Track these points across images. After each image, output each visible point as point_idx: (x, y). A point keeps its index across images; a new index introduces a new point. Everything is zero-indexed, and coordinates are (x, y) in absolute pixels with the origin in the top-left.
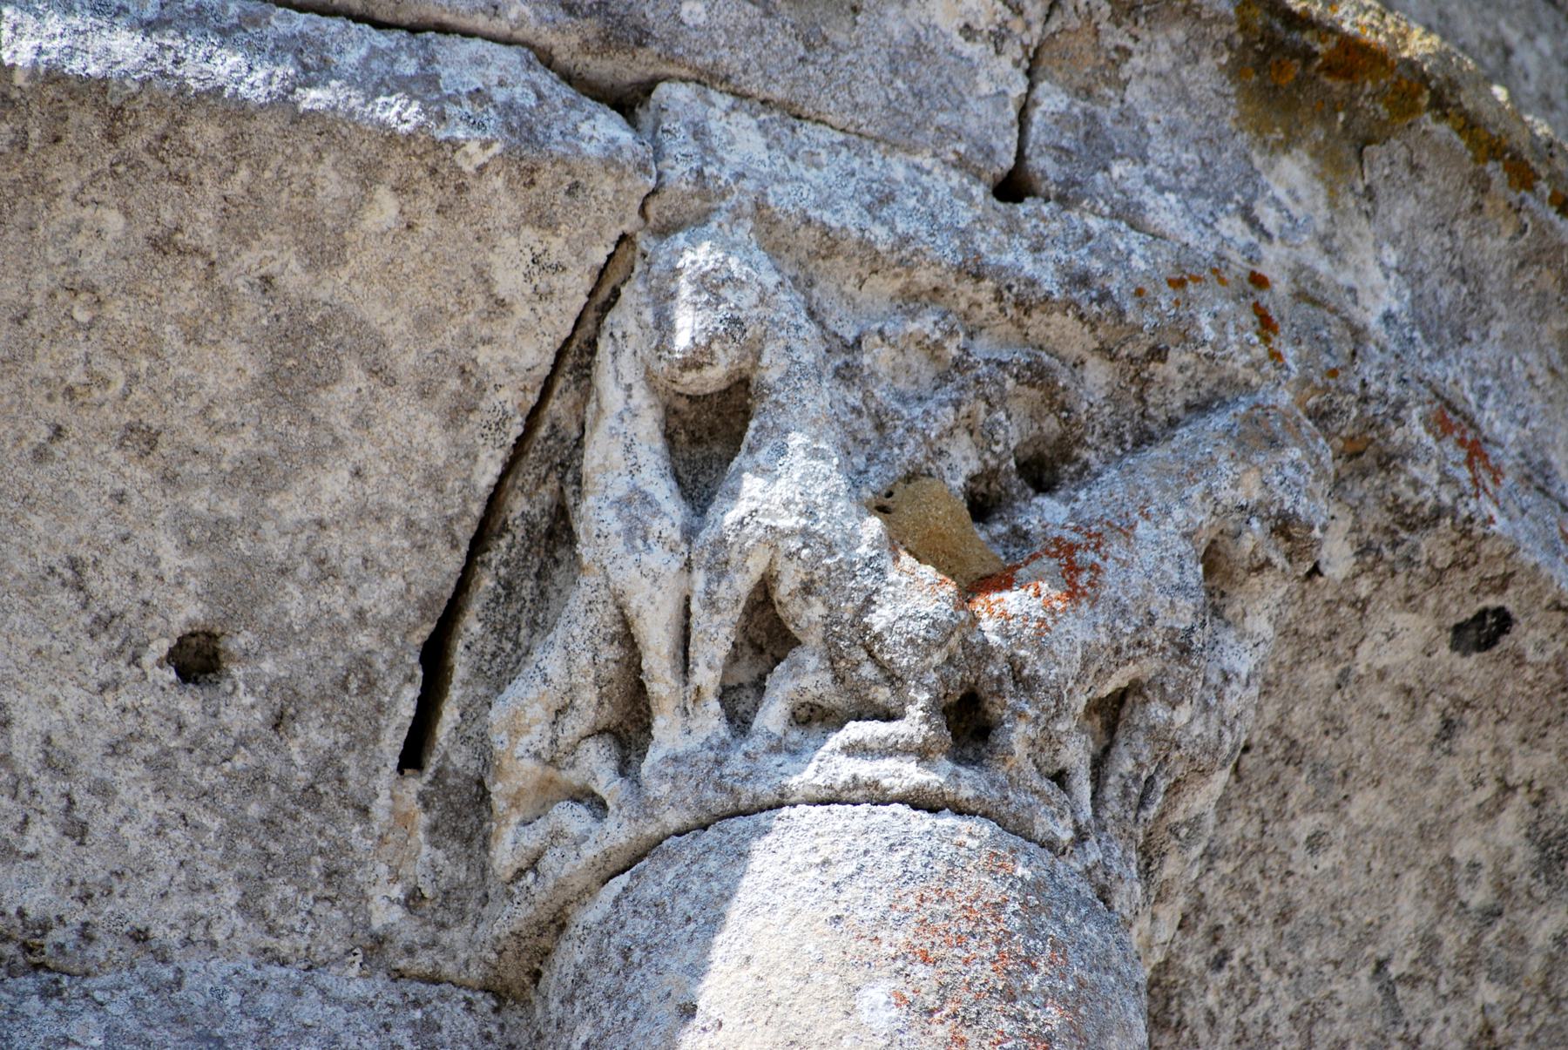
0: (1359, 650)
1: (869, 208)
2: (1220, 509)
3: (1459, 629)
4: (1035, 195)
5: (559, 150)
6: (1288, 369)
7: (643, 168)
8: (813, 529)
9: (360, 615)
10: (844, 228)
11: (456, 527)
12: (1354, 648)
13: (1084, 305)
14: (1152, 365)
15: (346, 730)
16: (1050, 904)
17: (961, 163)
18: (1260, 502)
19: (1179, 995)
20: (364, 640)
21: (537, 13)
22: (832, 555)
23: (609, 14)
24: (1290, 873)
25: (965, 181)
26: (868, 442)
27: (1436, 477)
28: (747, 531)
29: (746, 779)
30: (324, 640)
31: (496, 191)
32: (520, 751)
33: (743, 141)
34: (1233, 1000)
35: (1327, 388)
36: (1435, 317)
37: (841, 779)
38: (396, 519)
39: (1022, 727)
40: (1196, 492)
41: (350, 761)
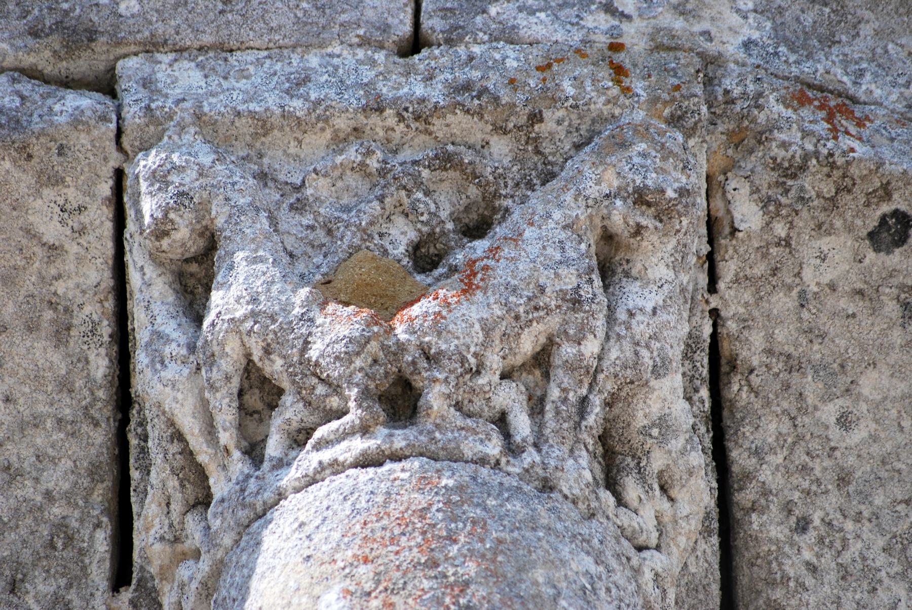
0: (803, 274)
1: (287, 92)
2: (590, 202)
3: (871, 235)
4: (430, 45)
5: (36, 128)
6: (638, 95)
7: (104, 118)
8: (257, 310)
9: (48, 495)
10: (267, 109)
11: (92, 412)
12: (798, 275)
13: (467, 103)
14: (536, 127)
15: (63, 575)
16: (471, 497)
17: (364, 42)
18: (619, 188)
19: (776, 559)
20: (57, 511)
21: (12, 45)
22: (274, 321)
23: (64, 28)
24: (833, 449)
25: (369, 52)
26: (324, 245)
27: (799, 135)
28: (217, 329)
29: (258, 493)
30: (29, 521)
31: (8, 171)
32: (151, 540)
33: (184, 78)
34: (826, 550)
35: (673, 99)
36: (800, 33)
37: (311, 469)
38: (49, 421)
39: (438, 388)
40: (569, 197)
41: (72, 595)
